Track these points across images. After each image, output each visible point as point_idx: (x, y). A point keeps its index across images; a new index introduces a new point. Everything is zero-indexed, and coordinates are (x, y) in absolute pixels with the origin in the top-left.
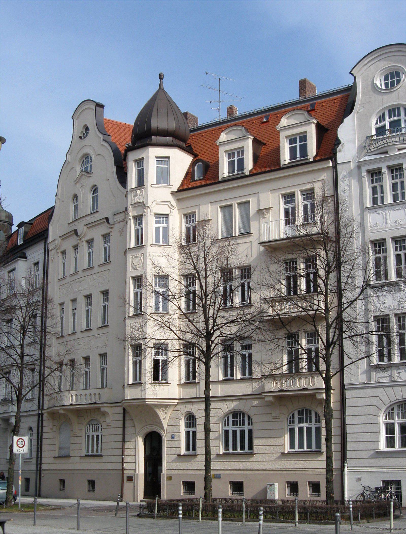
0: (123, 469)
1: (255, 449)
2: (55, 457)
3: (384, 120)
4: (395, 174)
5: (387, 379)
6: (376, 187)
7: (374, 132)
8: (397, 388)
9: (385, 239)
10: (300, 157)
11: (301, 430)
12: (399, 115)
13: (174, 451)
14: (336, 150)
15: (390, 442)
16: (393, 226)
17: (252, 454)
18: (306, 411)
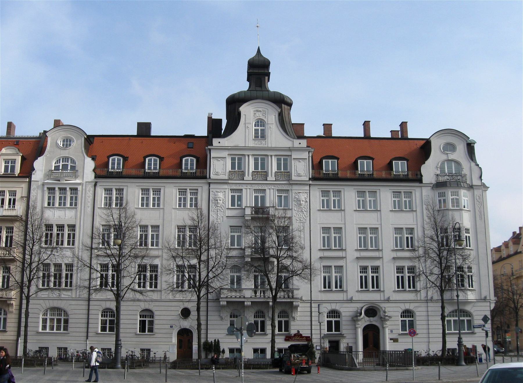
4: (61, 192)
5: (46, 296)
6: (51, 196)
7: (53, 169)
8: (51, 301)
10: (10, 172)
12: (68, 162)
14: (32, 173)
15: (44, 327)
16: (58, 219)
18: (284, 311)
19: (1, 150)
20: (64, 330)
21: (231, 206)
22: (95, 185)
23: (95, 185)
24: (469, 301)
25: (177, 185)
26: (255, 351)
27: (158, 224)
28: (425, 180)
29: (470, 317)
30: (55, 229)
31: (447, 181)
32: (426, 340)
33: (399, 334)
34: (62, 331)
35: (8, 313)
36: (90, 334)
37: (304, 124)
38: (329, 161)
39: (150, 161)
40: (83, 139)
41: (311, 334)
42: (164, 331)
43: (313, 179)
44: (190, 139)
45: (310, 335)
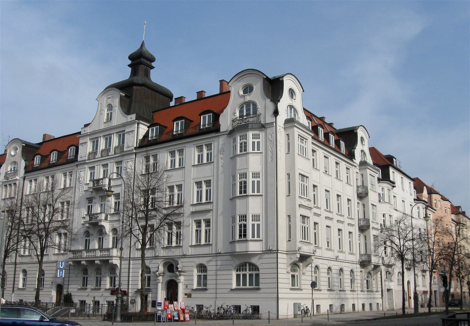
1: (261, 286)
13: (135, 287)
17: (259, 289)
21: (252, 151)
23: (24, 179)
24: (249, 252)
28: (222, 130)
32: (214, 296)
33: (193, 290)
40: (262, 80)
41: (128, 289)
45: (126, 290)
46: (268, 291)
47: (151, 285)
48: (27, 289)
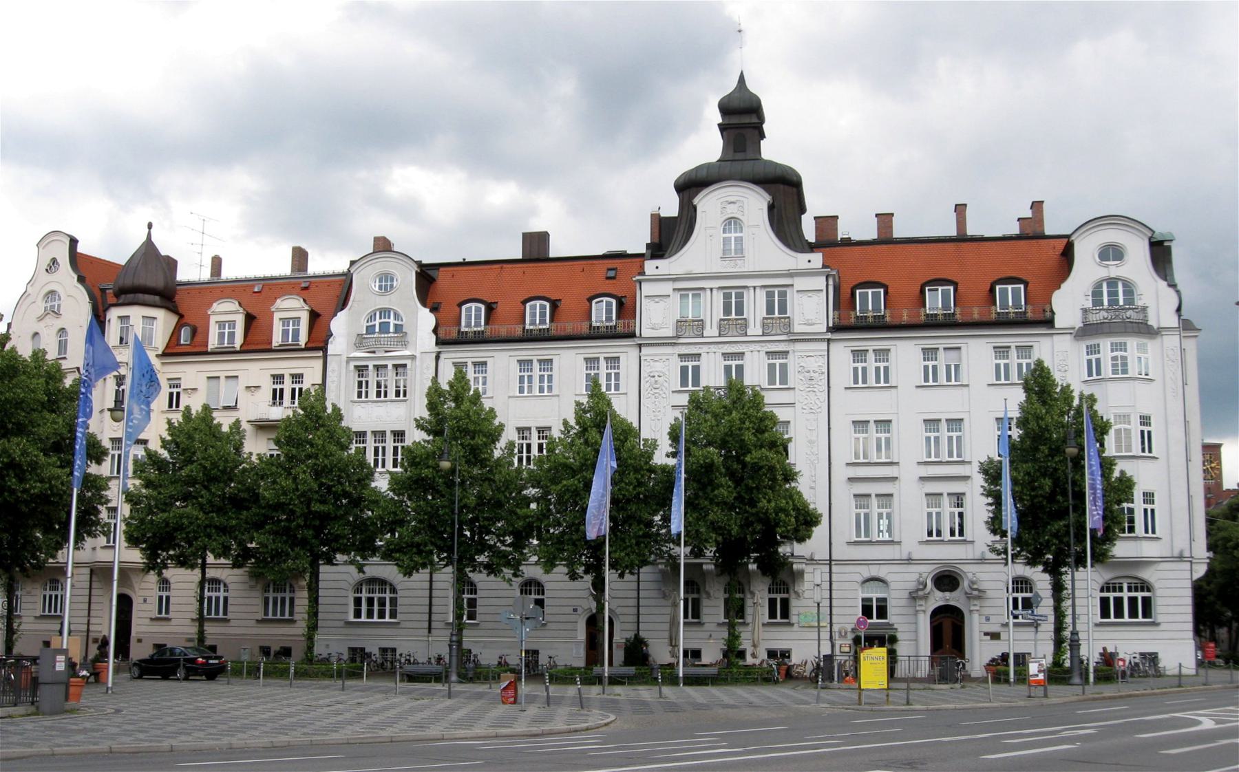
0: (88, 630)
2: (257, 620)
3: (375, 320)
9: (366, 432)
11: (275, 600)
15: (358, 614)
19: (275, 302)
20: (1144, 616)
22: (437, 358)
23: (437, 358)
25: (582, 351)
26: (772, 654)
27: (788, 420)
28: (1059, 322)
29: (1149, 590)
30: (370, 438)
31: (1103, 323)
34: (387, 619)
35: (296, 589)
36: (434, 625)
37: (837, 217)
38: (867, 293)
39: (533, 308)
42: (563, 618)
43: (836, 329)
44: (610, 261)
46: (1174, 626)
47: (171, 613)
48: (483, 625)
